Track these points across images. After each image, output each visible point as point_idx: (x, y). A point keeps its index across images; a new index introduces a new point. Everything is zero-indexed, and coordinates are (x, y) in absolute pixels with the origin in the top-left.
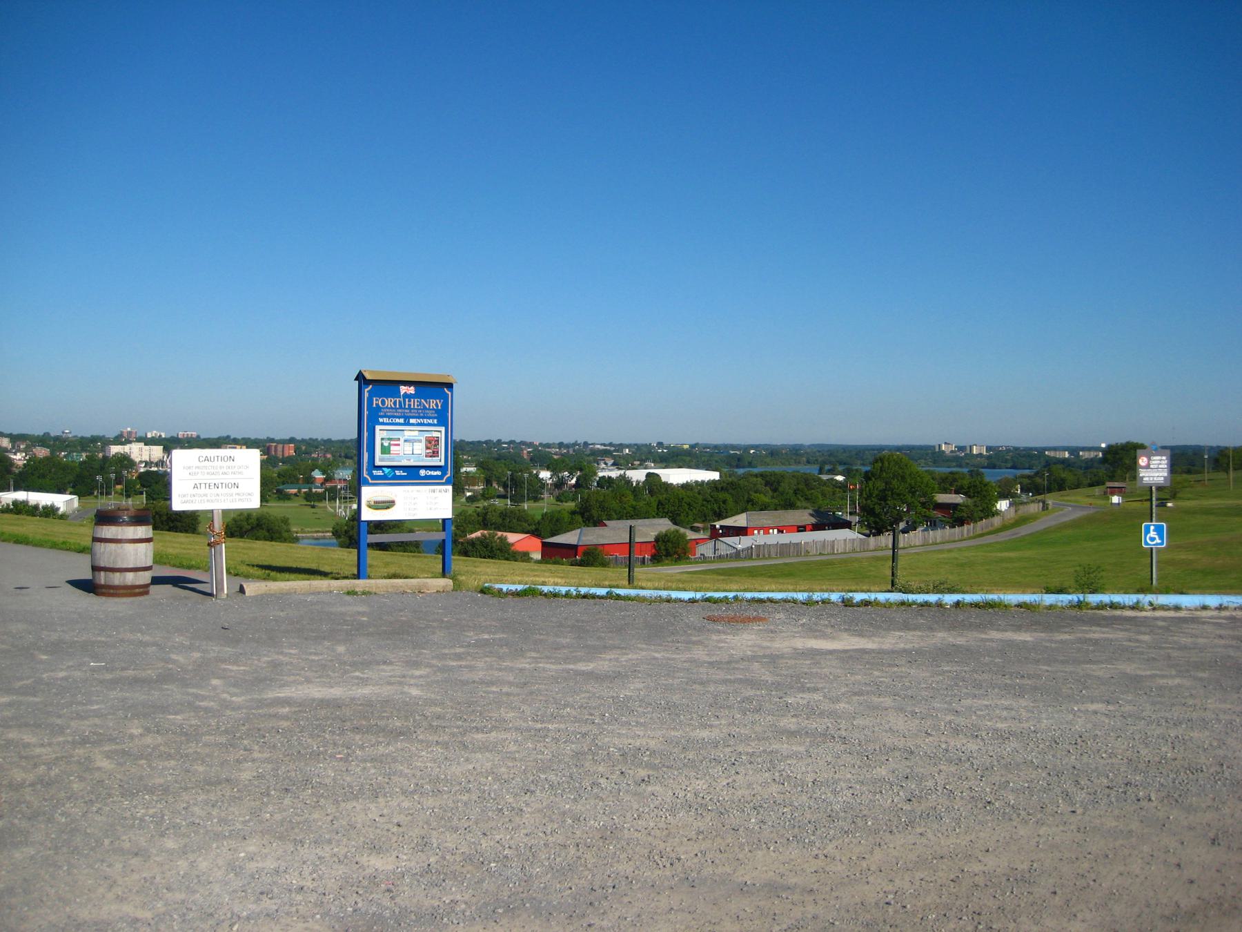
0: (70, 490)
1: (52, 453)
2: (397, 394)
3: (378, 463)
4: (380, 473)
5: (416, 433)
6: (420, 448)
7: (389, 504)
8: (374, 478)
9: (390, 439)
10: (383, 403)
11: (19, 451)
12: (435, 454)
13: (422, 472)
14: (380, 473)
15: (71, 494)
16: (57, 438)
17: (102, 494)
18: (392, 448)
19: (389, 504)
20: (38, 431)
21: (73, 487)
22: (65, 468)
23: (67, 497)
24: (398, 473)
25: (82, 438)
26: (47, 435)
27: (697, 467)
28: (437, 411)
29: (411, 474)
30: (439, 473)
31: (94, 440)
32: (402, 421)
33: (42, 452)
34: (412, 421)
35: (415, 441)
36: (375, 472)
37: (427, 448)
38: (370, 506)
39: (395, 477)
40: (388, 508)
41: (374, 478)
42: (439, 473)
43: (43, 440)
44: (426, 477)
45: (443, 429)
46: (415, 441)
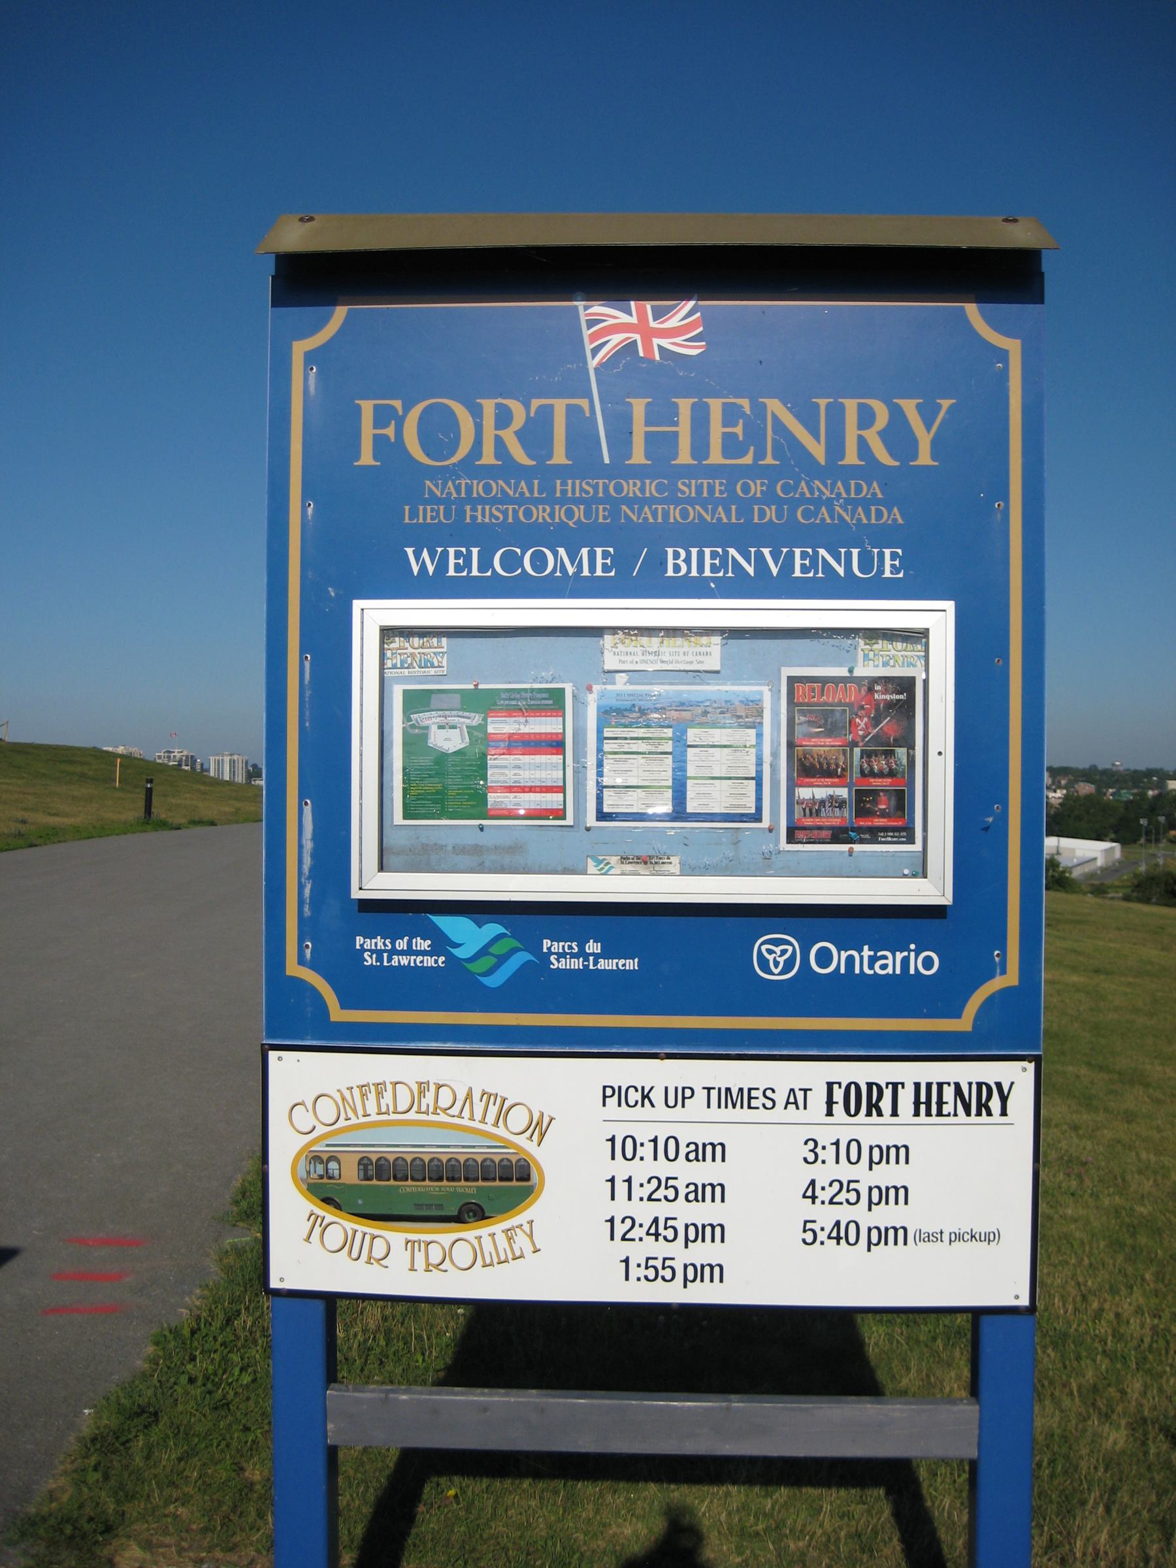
0: (1113, 836)
1: (1098, 790)
2: (562, 365)
3: (372, 882)
4: (413, 953)
5: (712, 654)
6: (735, 766)
7: (484, 1187)
8: (363, 985)
9: (482, 702)
10: (438, 429)
11: (1060, 787)
12: (879, 813)
13: (775, 956)
14: (413, 953)
15: (1113, 841)
16: (1105, 772)
17: (1149, 841)
18: (503, 769)
19: (484, 1187)
20: (1083, 764)
21: (1116, 832)
22: (1106, 808)
23: (1106, 845)
24: (561, 954)
25: (1135, 771)
26: (1093, 769)
27: (302, 635)
28: (900, 483)
29: (675, 978)
30: (922, 962)
31: (1149, 773)
32: (596, 561)
33: (1085, 789)
34: (676, 562)
35: (707, 714)
36: (370, 946)
37: (806, 768)
38: (326, 1192)
39: (537, 987)
40: (471, 1213)
41: (363, 985)
42: (922, 962)
43: (1088, 775)
44: (807, 993)
45: (938, 618)
46: (707, 714)
